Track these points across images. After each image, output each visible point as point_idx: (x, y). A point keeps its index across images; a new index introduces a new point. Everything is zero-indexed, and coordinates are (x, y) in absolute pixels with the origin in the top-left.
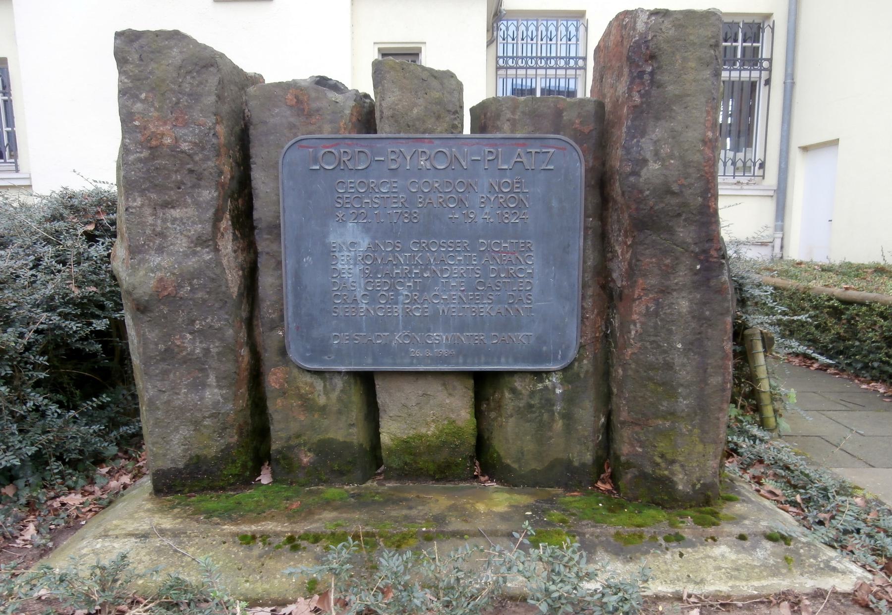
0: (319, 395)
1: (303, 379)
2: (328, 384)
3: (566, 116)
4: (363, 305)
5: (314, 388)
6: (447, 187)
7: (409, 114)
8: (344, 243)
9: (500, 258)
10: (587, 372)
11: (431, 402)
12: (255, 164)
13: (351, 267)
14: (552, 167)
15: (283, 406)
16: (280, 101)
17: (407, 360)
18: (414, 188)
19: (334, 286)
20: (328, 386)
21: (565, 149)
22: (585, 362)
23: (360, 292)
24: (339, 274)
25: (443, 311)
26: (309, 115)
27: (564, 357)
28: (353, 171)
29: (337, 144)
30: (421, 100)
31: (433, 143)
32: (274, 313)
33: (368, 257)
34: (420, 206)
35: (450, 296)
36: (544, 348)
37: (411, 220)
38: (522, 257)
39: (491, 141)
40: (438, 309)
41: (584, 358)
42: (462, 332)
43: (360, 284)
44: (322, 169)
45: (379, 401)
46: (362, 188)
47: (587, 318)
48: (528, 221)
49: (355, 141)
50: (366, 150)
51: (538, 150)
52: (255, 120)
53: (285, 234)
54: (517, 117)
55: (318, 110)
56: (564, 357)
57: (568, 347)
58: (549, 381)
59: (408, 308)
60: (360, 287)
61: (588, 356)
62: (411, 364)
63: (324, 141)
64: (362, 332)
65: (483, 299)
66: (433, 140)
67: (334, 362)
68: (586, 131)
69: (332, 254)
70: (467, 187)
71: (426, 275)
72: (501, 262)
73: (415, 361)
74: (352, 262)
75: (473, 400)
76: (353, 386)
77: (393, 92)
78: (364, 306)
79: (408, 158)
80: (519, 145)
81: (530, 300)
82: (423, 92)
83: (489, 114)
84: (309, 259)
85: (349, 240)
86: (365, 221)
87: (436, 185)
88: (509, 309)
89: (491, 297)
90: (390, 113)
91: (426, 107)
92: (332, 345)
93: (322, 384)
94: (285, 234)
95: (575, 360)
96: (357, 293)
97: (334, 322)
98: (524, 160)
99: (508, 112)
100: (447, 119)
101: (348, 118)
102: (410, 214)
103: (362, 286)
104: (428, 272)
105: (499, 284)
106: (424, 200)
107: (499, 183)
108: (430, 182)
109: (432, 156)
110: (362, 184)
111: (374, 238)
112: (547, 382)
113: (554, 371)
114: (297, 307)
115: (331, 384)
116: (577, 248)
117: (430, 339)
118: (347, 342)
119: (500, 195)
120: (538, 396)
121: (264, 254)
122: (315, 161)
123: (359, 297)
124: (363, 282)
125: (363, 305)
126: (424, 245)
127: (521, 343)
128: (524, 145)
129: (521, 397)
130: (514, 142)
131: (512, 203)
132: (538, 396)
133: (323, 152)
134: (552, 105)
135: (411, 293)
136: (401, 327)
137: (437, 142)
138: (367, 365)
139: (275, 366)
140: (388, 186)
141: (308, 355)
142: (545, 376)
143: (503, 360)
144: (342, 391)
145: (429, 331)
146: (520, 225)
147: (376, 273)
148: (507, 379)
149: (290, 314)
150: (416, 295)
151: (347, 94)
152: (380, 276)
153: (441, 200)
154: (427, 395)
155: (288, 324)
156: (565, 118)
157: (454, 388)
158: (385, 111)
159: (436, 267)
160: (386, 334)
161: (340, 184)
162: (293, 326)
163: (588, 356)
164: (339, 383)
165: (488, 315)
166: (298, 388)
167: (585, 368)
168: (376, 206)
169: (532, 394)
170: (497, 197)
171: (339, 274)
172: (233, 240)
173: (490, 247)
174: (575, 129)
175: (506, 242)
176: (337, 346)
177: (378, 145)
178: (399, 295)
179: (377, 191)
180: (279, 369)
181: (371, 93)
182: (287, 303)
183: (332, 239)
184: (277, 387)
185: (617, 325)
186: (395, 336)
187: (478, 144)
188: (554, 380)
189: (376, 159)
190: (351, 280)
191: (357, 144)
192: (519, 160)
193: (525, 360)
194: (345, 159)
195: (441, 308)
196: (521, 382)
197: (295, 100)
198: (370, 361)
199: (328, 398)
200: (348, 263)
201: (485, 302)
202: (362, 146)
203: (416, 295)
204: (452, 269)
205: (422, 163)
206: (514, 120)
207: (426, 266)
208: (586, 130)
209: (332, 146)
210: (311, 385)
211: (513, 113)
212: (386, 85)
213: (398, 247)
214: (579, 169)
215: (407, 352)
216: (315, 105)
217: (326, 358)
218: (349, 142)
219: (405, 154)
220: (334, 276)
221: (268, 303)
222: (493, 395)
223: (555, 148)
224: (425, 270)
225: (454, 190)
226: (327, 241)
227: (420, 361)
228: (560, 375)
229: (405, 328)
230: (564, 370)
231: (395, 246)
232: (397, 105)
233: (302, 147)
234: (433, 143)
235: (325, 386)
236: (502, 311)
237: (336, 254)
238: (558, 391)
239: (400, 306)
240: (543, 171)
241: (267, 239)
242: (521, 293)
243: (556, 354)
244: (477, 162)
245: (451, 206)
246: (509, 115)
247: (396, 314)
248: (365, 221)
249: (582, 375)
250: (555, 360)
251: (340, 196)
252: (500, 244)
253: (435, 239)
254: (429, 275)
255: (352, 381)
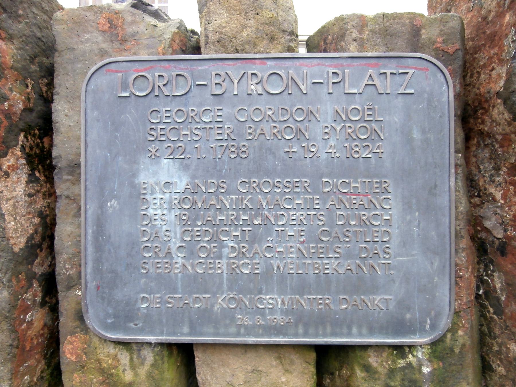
0: (124, 370)
1: (106, 350)
2: (135, 356)
3: (424, 35)
4: (179, 259)
5: (119, 361)
6: (283, 116)
7: (238, 37)
8: (157, 184)
9: (349, 201)
10: (463, 345)
11: (263, 379)
12: (58, 94)
13: (165, 212)
14: (412, 91)
15: (80, 381)
16: (91, 26)
17: (233, 330)
18: (242, 116)
19: (144, 236)
20: (135, 360)
21: (427, 70)
22: (460, 332)
23: (175, 243)
24: (150, 222)
25: (278, 267)
26: (124, 41)
27: (433, 327)
28: (169, 98)
29: (152, 67)
30: (252, 21)
31: (265, 64)
32: (72, 268)
33: (186, 200)
34: (250, 138)
35: (286, 248)
36: (408, 316)
37: (238, 155)
38: (377, 199)
39: (336, 61)
40: (272, 265)
41: (459, 328)
42: (302, 295)
43: (175, 233)
44: (133, 96)
45: (199, 378)
46: (180, 117)
47: (461, 277)
48: (383, 156)
49: (172, 64)
50: (185, 74)
51: (394, 71)
52: (60, 45)
53: (86, 174)
54: (365, 36)
55: (134, 35)
56: (433, 327)
57: (438, 315)
58: (413, 356)
59: (234, 263)
60: (176, 237)
61: (463, 326)
62: (238, 335)
63: (136, 64)
64: (176, 293)
65: (327, 253)
66: (265, 61)
67: (141, 331)
68: (451, 51)
69: (142, 197)
70: (307, 115)
71: (256, 222)
72: (350, 206)
73: (242, 331)
74: (166, 206)
75: (315, 377)
76: (166, 359)
77: (220, 14)
78: (180, 260)
79: (236, 82)
80: (370, 66)
81: (388, 253)
82: (254, 12)
83: (330, 38)
84: (114, 202)
85: (163, 179)
86: (183, 157)
87: (270, 113)
88: (362, 266)
89: (338, 250)
90: (216, 37)
91: (257, 29)
92: (139, 309)
93: (128, 357)
94: (86, 174)
95: (448, 331)
96: (171, 245)
97: (143, 280)
98: (377, 82)
99: (354, 31)
100: (282, 40)
101: (168, 43)
102: (238, 148)
103: (178, 235)
104: (260, 218)
105: (348, 234)
106: (255, 131)
107: (347, 110)
108: (262, 109)
109: (265, 78)
110: (180, 113)
111: (194, 177)
112: (411, 358)
113: (421, 346)
114: (98, 261)
115: (139, 356)
116: (447, 189)
117: (261, 303)
118: (158, 305)
119: (348, 125)
120: (399, 376)
121: (63, 197)
122: (125, 87)
123: (174, 250)
124: (179, 230)
125: (179, 259)
126: (254, 185)
127: (378, 309)
128: (376, 65)
129: (377, 376)
130: (364, 62)
131: (363, 134)
132: (399, 376)
133: (134, 77)
134: (407, 22)
135: (238, 244)
136: (225, 287)
137: (270, 63)
138: (183, 334)
139: (72, 333)
140: (212, 114)
141: (109, 321)
142: (407, 350)
143: (355, 330)
144: (152, 365)
145: (260, 293)
146: (373, 161)
147: (195, 220)
148: (359, 353)
149: (89, 271)
150: (244, 247)
151: (170, 23)
152: (200, 223)
153: (275, 131)
154: (258, 371)
155: (86, 282)
156: (423, 37)
157: (292, 363)
158: (210, 35)
159: (269, 212)
160: (207, 296)
161: (154, 113)
162: (92, 285)
163: (463, 326)
164: (149, 356)
165: (335, 272)
166: (99, 361)
167: (461, 341)
168: (197, 138)
169: (392, 373)
170: (344, 126)
171: (150, 222)
172: (28, 182)
173: (337, 187)
174: (437, 49)
175: (356, 182)
176: (145, 311)
177: (200, 68)
178: (223, 247)
179: (198, 120)
180: (76, 337)
181: (198, 29)
182: (86, 256)
183: (142, 178)
184: (73, 359)
185: (498, 285)
186: (218, 298)
187: (319, 64)
188: (420, 355)
189: (197, 83)
190: (165, 228)
191: (175, 67)
192: (370, 82)
193: (384, 330)
194: (161, 84)
195: (275, 263)
196: (377, 357)
197: (108, 25)
198: (186, 330)
199: (136, 374)
200: (161, 208)
201: (330, 256)
202: (180, 69)
203: (244, 247)
204: (289, 215)
205: (252, 87)
206: (362, 39)
207: (257, 211)
208: (451, 49)
209: (145, 70)
210: (115, 358)
211: (361, 32)
212: (212, 7)
213: (223, 188)
214: (446, 94)
215: (233, 319)
216: (130, 30)
217: (132, 325)
218: (166, 64)
219: (232, 77)
220: (144, 223)
221: (65, 257)
222: (340, 370)
223: (415, 68)
224: (255, 217)
225: (291, 119)
226: (137, 181)
227: (249, 330)
228: (427, 350)
229: (230, 289)
230: (434, 344)
231: (219, 187)
232: (224, 27)
233: (109, 71)
234: (265, 64)
235: (131, 359)
236: (353, 267)
237: (148, 197)
238: (426, 370)
239: (224, 261)
240: (400, 95)
241: (68, 180)
242: (377, 246)
243: (423, 323)
244: (318, 85)
245: (288, 138)
246: (355, 34)
247: (220, 271)
248: (183, 157)
249: (457, 350)
250: (423, 331)
251: (154, 127)
252: (348, 184)
253: (268, 177)
254: (260, 222)
255: (166, 353)
